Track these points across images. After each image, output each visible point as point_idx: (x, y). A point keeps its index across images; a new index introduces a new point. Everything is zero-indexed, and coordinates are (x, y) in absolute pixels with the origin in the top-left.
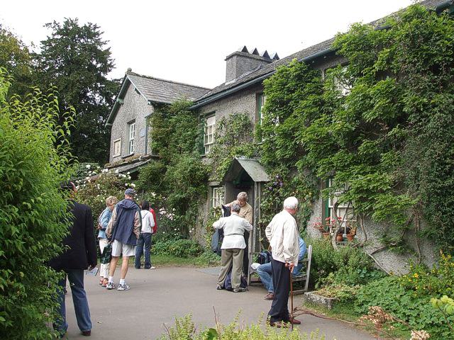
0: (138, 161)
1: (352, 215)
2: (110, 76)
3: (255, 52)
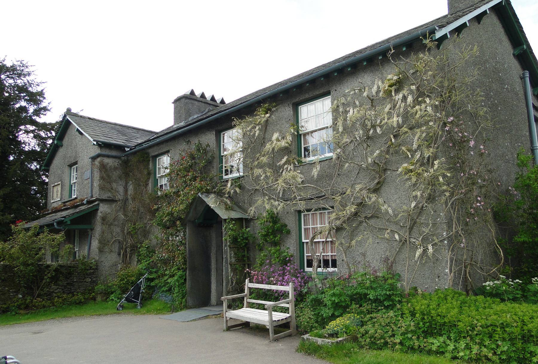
0: (83, 204)
3: (203, 96)
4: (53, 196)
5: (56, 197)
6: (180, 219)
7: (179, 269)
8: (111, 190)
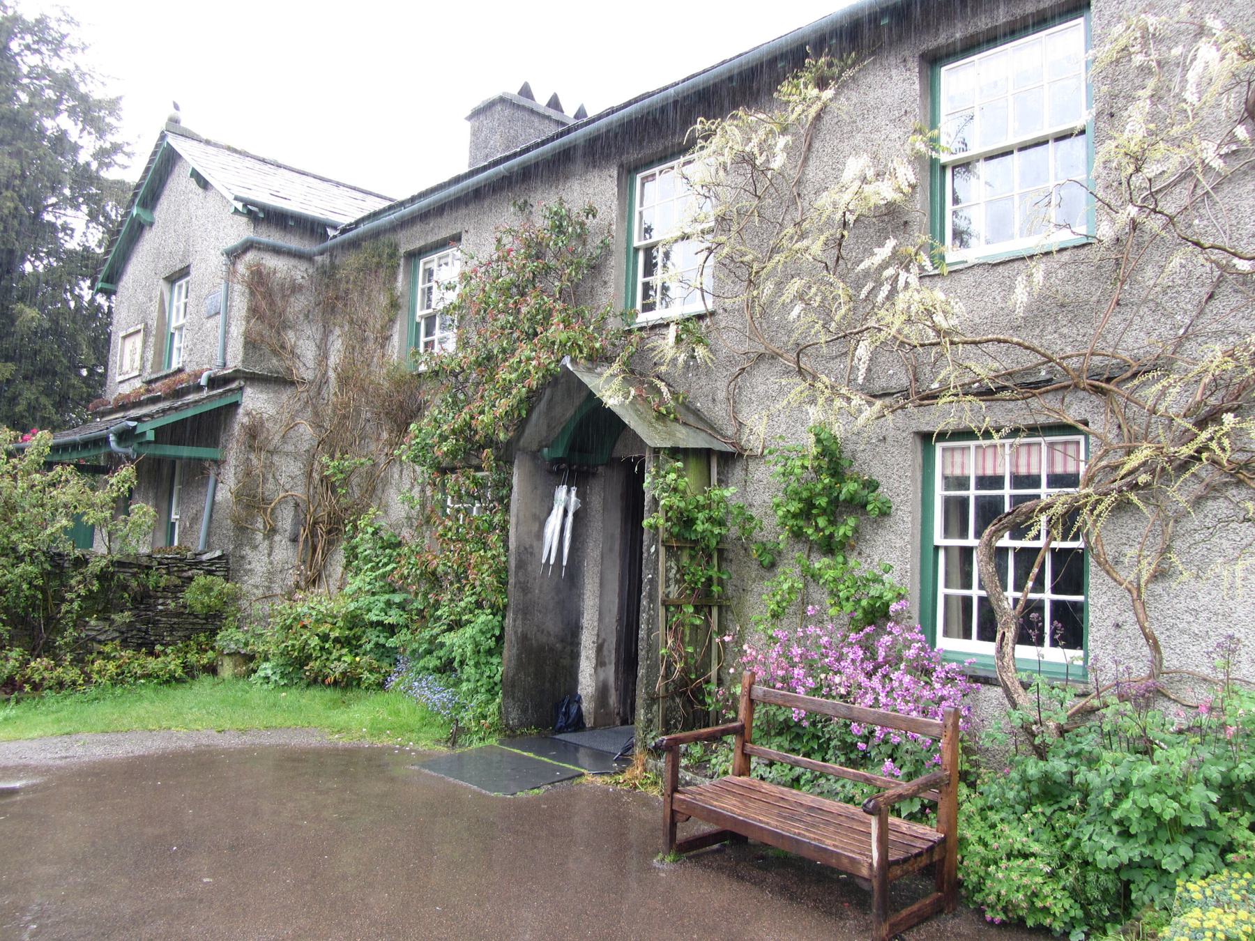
0: (199, 388)
3: (554, 103)
4: (121, 366)
5: (128, 366)
6: (490, 442)
7: (479, 605)
8: (280, 349)
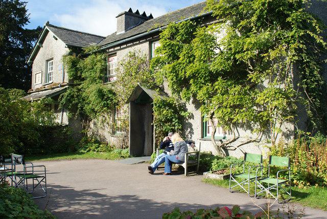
0: (58, 87)
1: (7, 200)
2: (25, 27)
